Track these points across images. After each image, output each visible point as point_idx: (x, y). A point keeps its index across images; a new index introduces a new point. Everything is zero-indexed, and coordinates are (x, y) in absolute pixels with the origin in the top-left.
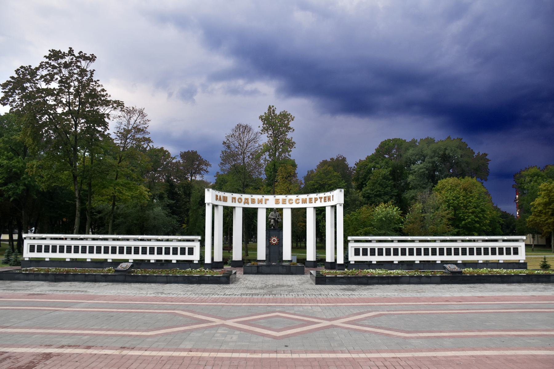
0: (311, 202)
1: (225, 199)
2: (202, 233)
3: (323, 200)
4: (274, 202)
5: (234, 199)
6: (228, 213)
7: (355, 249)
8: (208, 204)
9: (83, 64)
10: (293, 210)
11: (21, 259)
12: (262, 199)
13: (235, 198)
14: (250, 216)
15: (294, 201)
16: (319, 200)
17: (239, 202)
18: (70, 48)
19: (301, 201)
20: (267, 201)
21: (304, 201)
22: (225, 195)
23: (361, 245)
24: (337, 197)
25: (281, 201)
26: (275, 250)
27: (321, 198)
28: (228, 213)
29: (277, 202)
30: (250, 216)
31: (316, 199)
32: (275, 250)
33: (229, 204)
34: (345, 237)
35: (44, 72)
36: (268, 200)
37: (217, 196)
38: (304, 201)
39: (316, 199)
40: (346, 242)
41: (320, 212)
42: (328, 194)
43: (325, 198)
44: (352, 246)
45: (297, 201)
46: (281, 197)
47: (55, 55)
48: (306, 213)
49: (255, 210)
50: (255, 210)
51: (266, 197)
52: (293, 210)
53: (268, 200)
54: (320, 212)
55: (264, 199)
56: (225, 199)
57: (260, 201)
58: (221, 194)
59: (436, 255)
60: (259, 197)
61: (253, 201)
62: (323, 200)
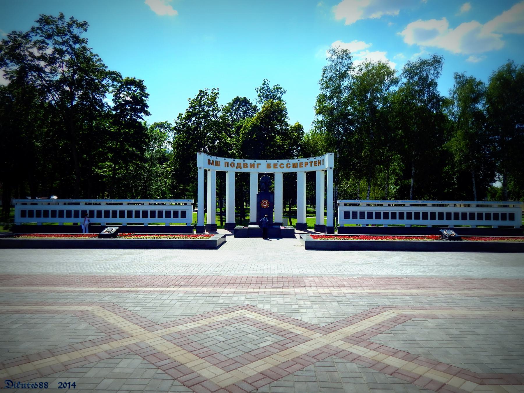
0: (301, 166)
1: (218, 164)
2: (195, 196)
3: (313, 164)
4: (265, 166)
5: (226, 164)
6: (221, 176)
7: (345, 212)
8: (200, 168)
9: (76, 31)
10: (285, 175)
11: (500, 192)
12: (254, 164)
13: (228, 163)
14: (242, 179)
15: (285, 166)
16: (309, 164)
17: (231, 167)
18: (62, 14)
19: (291, 165)
20: (259, 166)
21: (295, 165)
22: (217, 160)
23: (351, 209)
24: (328, 160)
25: (272, 165)
26: (265, 212)
27: (311, 162)
28: (221, 176)
29: (269, 166)
30: (242, 179)
31: (306, 164)
32: (265, 212)
33: (222, 169)
34: (335, 202)
35: (35, 38)
36: (260, 164)
37: (209, 160)
38: (295, 165)
39: (306, 164)
40: (336, 206)
41: (311, 177)
42: (318, 158)
43: (315, 162)
44: (341, 210)
45: (288, 166)
46: (272, 162)
47: (45, 21)
48: (296, 178)
49: (247, 175)
50: (247, 175)
51: (258, 161)
52: (285, 175)
53: (260, 164)
54: (311, 177)
55: (256, 164)
56: (218, 164)
57: (252, 166)
58: (213, 158)
59: (459, 219)
60: (252, 161)
61: (246, 166)
62: (313, 164)
